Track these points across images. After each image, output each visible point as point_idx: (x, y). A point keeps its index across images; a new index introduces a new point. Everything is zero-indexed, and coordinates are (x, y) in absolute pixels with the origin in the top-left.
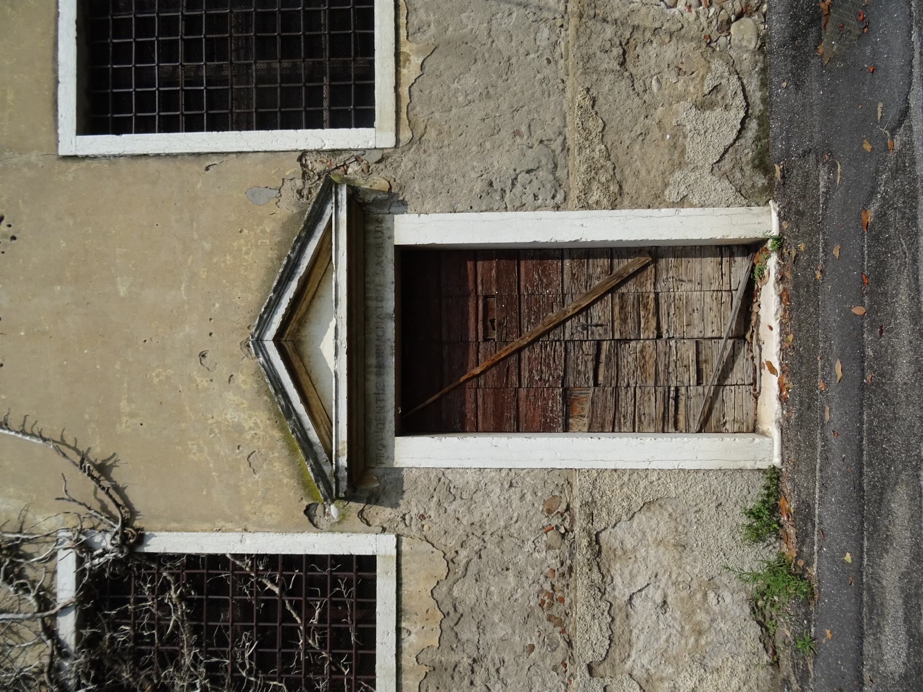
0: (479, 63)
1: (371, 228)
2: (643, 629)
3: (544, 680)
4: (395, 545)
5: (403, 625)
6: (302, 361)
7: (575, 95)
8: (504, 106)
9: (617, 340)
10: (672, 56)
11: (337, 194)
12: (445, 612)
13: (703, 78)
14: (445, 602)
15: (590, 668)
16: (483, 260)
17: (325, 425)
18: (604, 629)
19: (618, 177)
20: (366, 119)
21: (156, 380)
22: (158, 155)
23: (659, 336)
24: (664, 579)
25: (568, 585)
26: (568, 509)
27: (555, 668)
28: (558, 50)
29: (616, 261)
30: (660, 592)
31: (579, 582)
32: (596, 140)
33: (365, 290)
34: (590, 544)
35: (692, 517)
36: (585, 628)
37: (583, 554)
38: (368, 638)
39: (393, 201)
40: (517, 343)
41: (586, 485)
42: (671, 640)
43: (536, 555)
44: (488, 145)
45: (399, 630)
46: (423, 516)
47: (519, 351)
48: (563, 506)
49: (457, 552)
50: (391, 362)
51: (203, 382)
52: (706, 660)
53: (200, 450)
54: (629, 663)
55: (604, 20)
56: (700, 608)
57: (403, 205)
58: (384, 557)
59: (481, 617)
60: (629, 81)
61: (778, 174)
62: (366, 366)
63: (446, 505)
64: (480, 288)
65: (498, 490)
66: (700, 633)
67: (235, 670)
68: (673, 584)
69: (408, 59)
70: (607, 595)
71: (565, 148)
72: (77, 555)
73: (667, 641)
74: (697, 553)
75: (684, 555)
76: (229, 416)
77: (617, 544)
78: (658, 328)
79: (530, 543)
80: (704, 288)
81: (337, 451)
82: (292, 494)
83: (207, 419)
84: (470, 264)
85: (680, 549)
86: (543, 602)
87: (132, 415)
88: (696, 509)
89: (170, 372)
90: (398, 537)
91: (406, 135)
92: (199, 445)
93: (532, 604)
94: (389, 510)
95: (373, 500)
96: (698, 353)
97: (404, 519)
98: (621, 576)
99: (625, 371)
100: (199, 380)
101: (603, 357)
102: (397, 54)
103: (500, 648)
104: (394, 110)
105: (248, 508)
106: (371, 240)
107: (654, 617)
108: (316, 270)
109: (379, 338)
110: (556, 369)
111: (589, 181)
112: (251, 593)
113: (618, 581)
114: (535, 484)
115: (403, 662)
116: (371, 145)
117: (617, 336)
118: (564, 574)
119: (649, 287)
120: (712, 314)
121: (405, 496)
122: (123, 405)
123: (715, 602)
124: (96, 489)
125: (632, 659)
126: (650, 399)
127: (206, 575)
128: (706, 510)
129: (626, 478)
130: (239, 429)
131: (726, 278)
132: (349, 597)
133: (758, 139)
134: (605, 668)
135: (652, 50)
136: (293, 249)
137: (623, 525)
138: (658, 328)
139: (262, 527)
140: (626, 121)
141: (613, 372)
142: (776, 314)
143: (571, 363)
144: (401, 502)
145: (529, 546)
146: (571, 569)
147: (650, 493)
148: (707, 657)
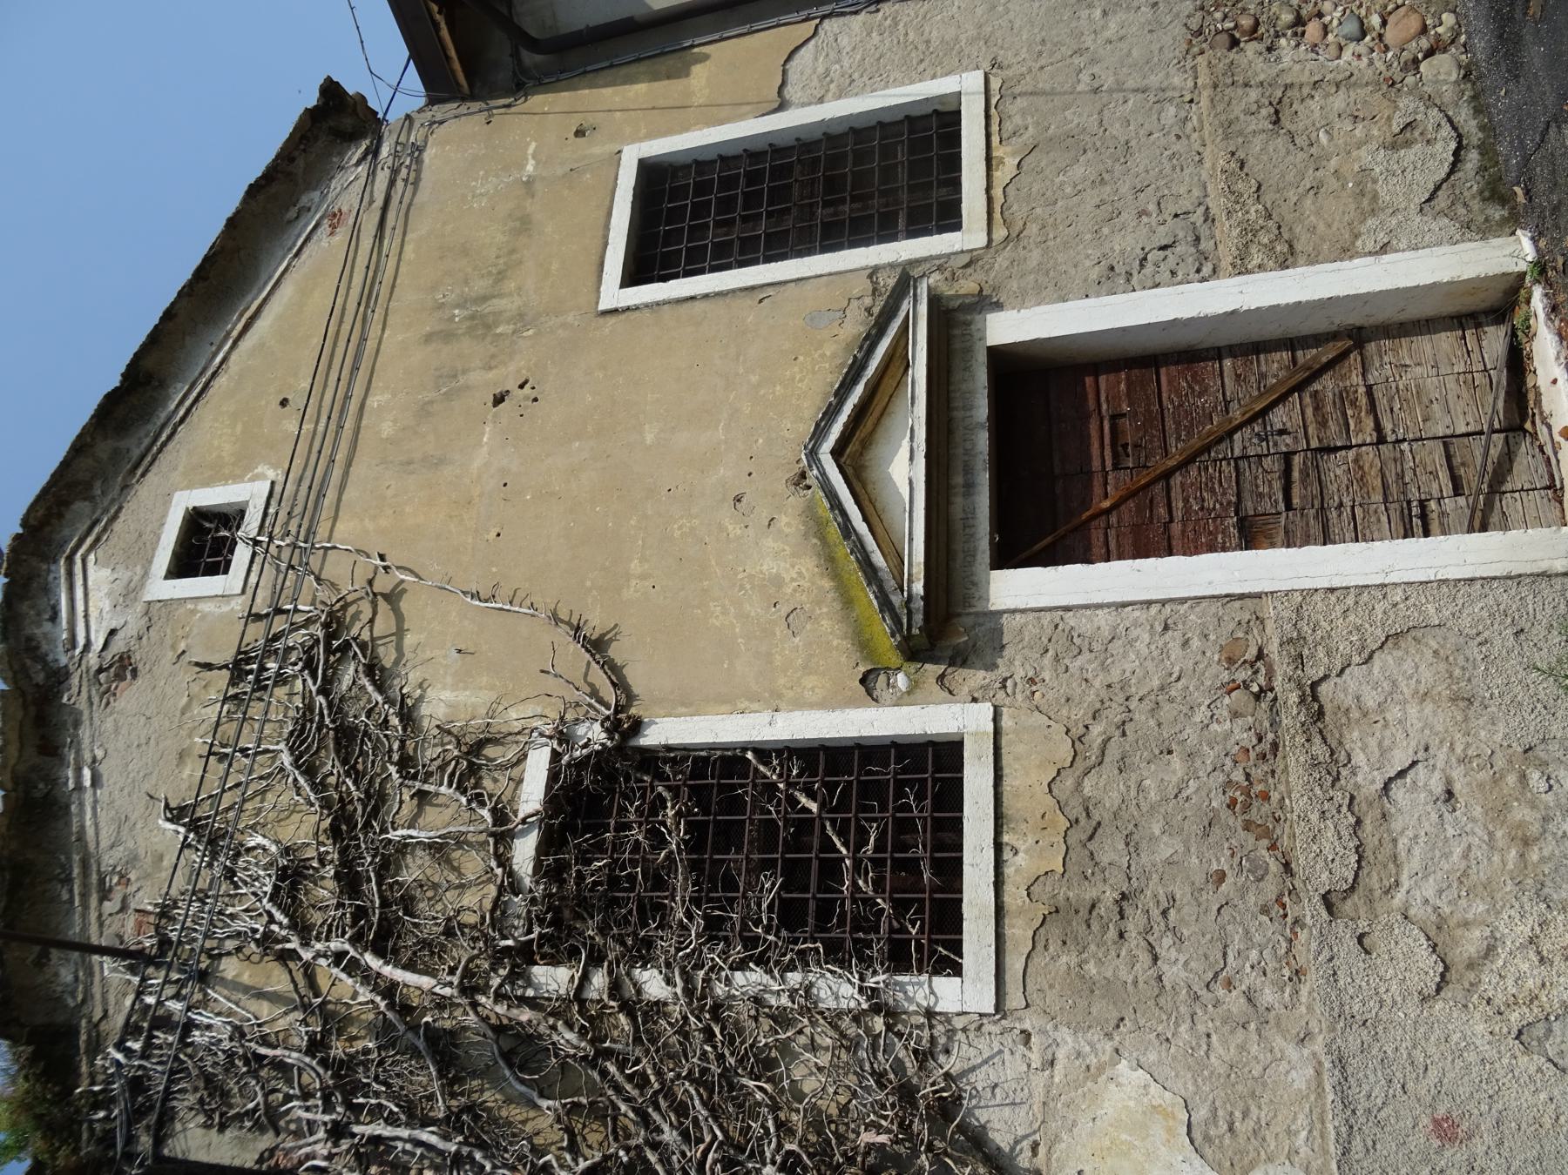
0: (1089, 153)
1: (957, 332)
2: (1416, 836)
3: (1247, 932)
4: (991, 716)
5: (1006, 838)
6: (864, 487)
7: (1216, 158)
8: (1125, 189)
9: (1316, 450)
10: (1343, 105)
11: (915, 289)
12: (1073, 818)
13: (1389, 119)
14: (1072, 803)
15: (1326, 899)
16: (1107, 372)
17: (896, 557)
18: (1345, 833)
19: (1286, 236)
20: (949, 218)
21: (677, 534)
22: (706, 296)
23: (1381, 440)
24: (1442, 755)
25: (1273, 772)
26: (1260, 655)
27: (1265, 910)
28: (1189, 126)
29: (1299, 353)
30: (1437, 775)
31: (1291, 761)
32: (1250, 202)
33: (948, 400)
34: (1302, 701)
35: (1474, 652)
36: (1311, 834)
37: (1292, 715)
38: (951, 871)
39: (986, 302)
40: (1159, 464)
41: (1286, 614)
42: (1472, 855)
43: (1215, 727)
44: (1106, 231)
45: (998, 847)
46: (1031, 680)
47: (1167, 475)
48: (1252, 653)
49: (1087, 727)
50: (984, 479)
51: (734, 529)
52: (1546, 890)
53: (725, 612)
54: (1399, 897)
55: (1246, 85)
56: (1517, 799)
57: (998, 306)
58: (975, 734)
59: (1131, 826)
60: (1288, 137)
61: (1521, 198)
62: (949, 487)
63: (1067, 661)
64: (1104, 407)
65: (1146, 637)
66: (1526, 842)
67: (745, 927)
68: (1461, 761)
69: (1001, 161)
70: (1343, 782)
71: (1208, 218)
72: (553, 750)
73: (1465, 856)
74: (1494, 709)
75: (1471, 713)
76: (765, 567)
77: (1349, 701)
78: (1378, 428)
79: (1203, 708)
80: (1443, 371)
81: (910, 575)
82: (843, 659)
83: (736, 574)
84: (1089, 380)
85: (1462, 704)
86: (1234, 802)
87: (643, 577)
88: (1479, 639)
89: (696, 522)
90: (995, 707)
91: (1000, 233)
92: (723, 606)
93: (1214, 804)
94: (982, 673)
95: (959, 661)
96: (1449, 457)
97: (1005, 687)
98: (1363, 749)
99: (1334, 487)
100: (730, 528)
101: (1296, 475)
102: (989, 159)
103: (1166, 877)
104: (985, 210)
105: (782, 681)
106: (957, 345)
107: (1434, 816)
108: (885, 380)
109: (967, 452)
110: (1224, 494)
111: (1246, 245)
112: (778, 812)
113: (1359, 758)
114: (1203, 624)
115: (1007, 899)
116: (957, 248)
117: (1314, 444)
118: (1264, 756)
119: (1356, 378)
120: (1462, 403)
121: (1005, 653)
122: (635, 566)
123: (1543, 786)
124: (589, 663)
125: (1403, 890)
126: (1379, 520)
127: (717, 774)
128: (1498, 642)
129: (1350, 601)
130: (777, 581)
131: (1475, 356)
132: (921, 812)
133: (1482, 169)
134: (1355, 905)
135: (1314, 105)
136: (861, 348)
137: (1354, 671)
138: (1378, 428)
139: (799, 704)
140: (1290, 177)
141: (1316, 490)
142: (1558, 358)
143: (1247, 486)
144: (999, 661)
145: (1201, 715)
146: (1275, 746)
147: (1397, 624)
148: (1548, 883)
